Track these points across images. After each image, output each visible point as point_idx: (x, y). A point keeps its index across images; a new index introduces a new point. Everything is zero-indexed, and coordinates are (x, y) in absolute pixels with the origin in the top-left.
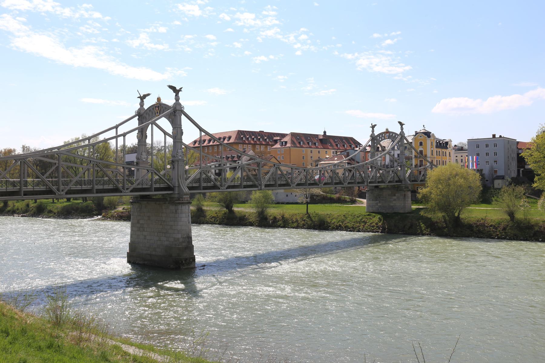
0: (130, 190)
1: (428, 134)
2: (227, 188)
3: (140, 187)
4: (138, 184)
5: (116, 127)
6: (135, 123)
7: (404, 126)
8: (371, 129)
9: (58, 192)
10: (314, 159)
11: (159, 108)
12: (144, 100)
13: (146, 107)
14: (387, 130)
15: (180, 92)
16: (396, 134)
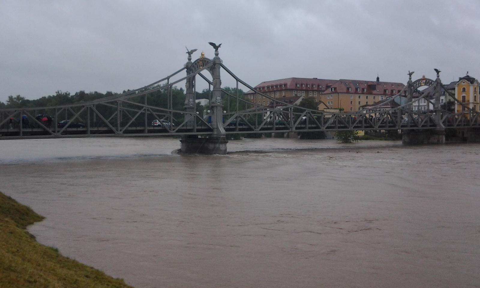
0: (175, 131)
1: (472, 80)
2: (260, 130)
3: (185, 128)
4: (183, 126)
5: (168, 78)
6: (184, 74)
7: (440, 73)
8: (409, 76)
9: (116, 131)
10: (362, 104)
11: (202, 62)
12: (192, 55)
13: (193, 61)
14: (424, 77)
15: (219, 48)
16: (432, 81)
